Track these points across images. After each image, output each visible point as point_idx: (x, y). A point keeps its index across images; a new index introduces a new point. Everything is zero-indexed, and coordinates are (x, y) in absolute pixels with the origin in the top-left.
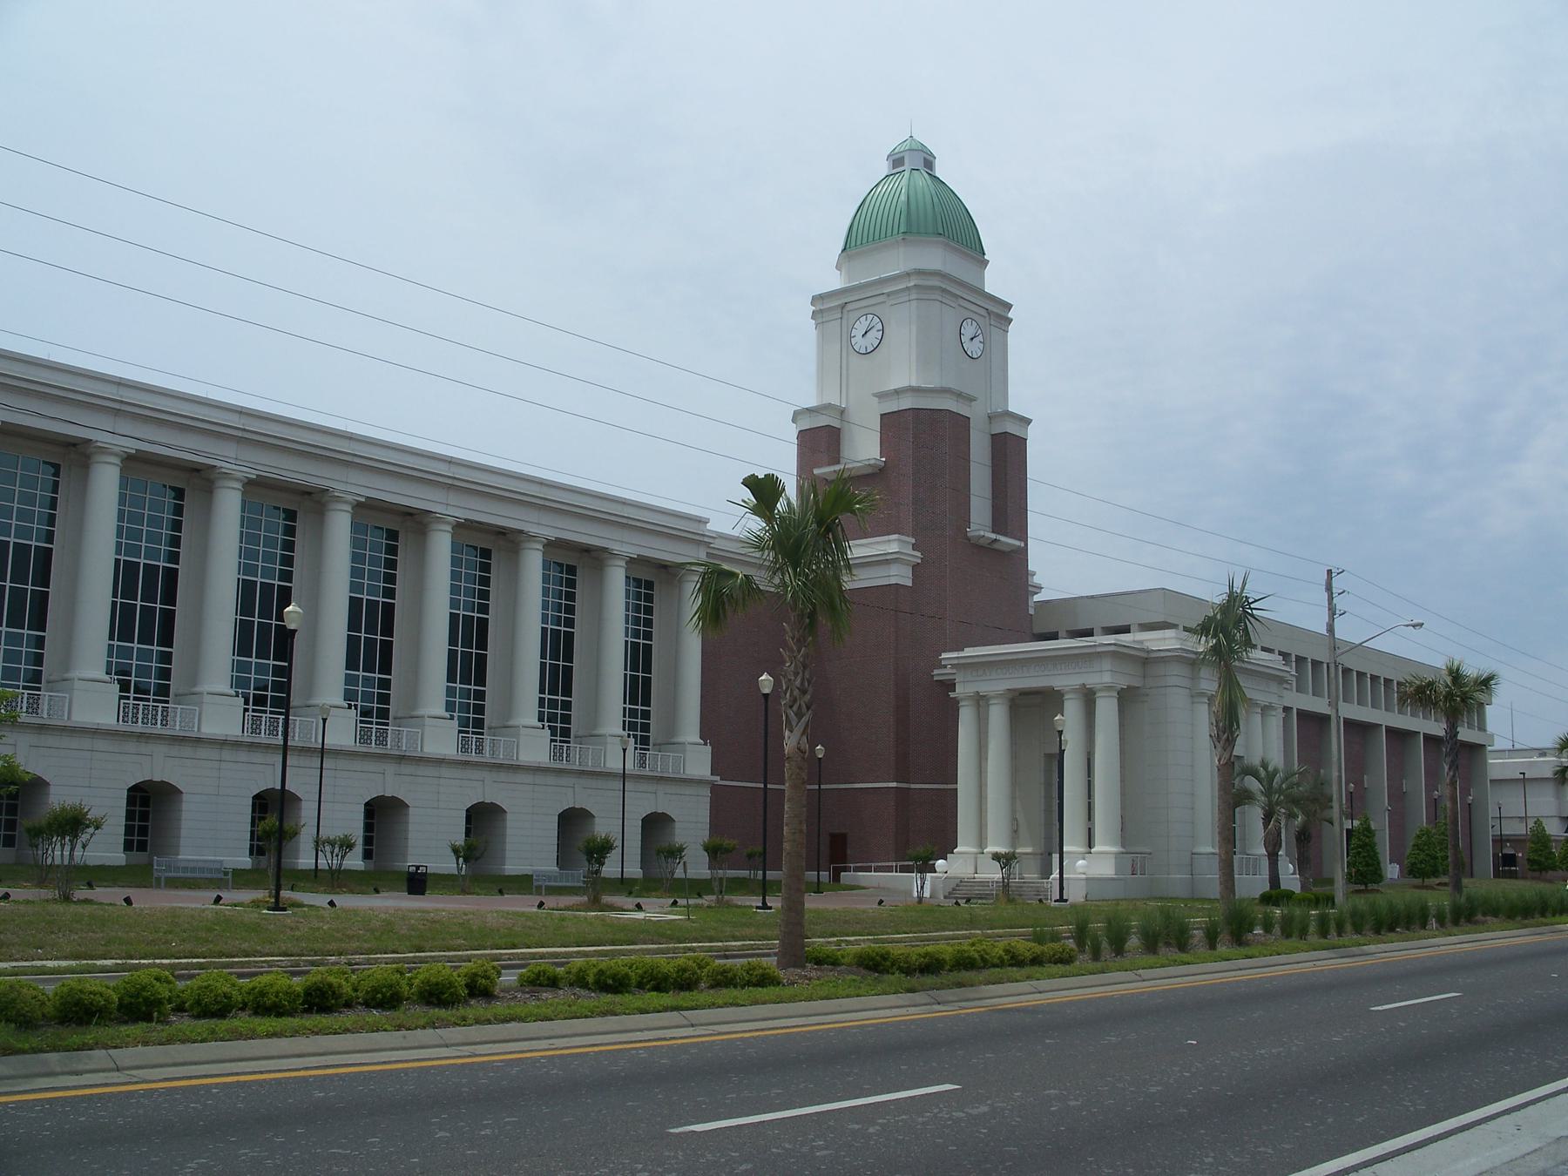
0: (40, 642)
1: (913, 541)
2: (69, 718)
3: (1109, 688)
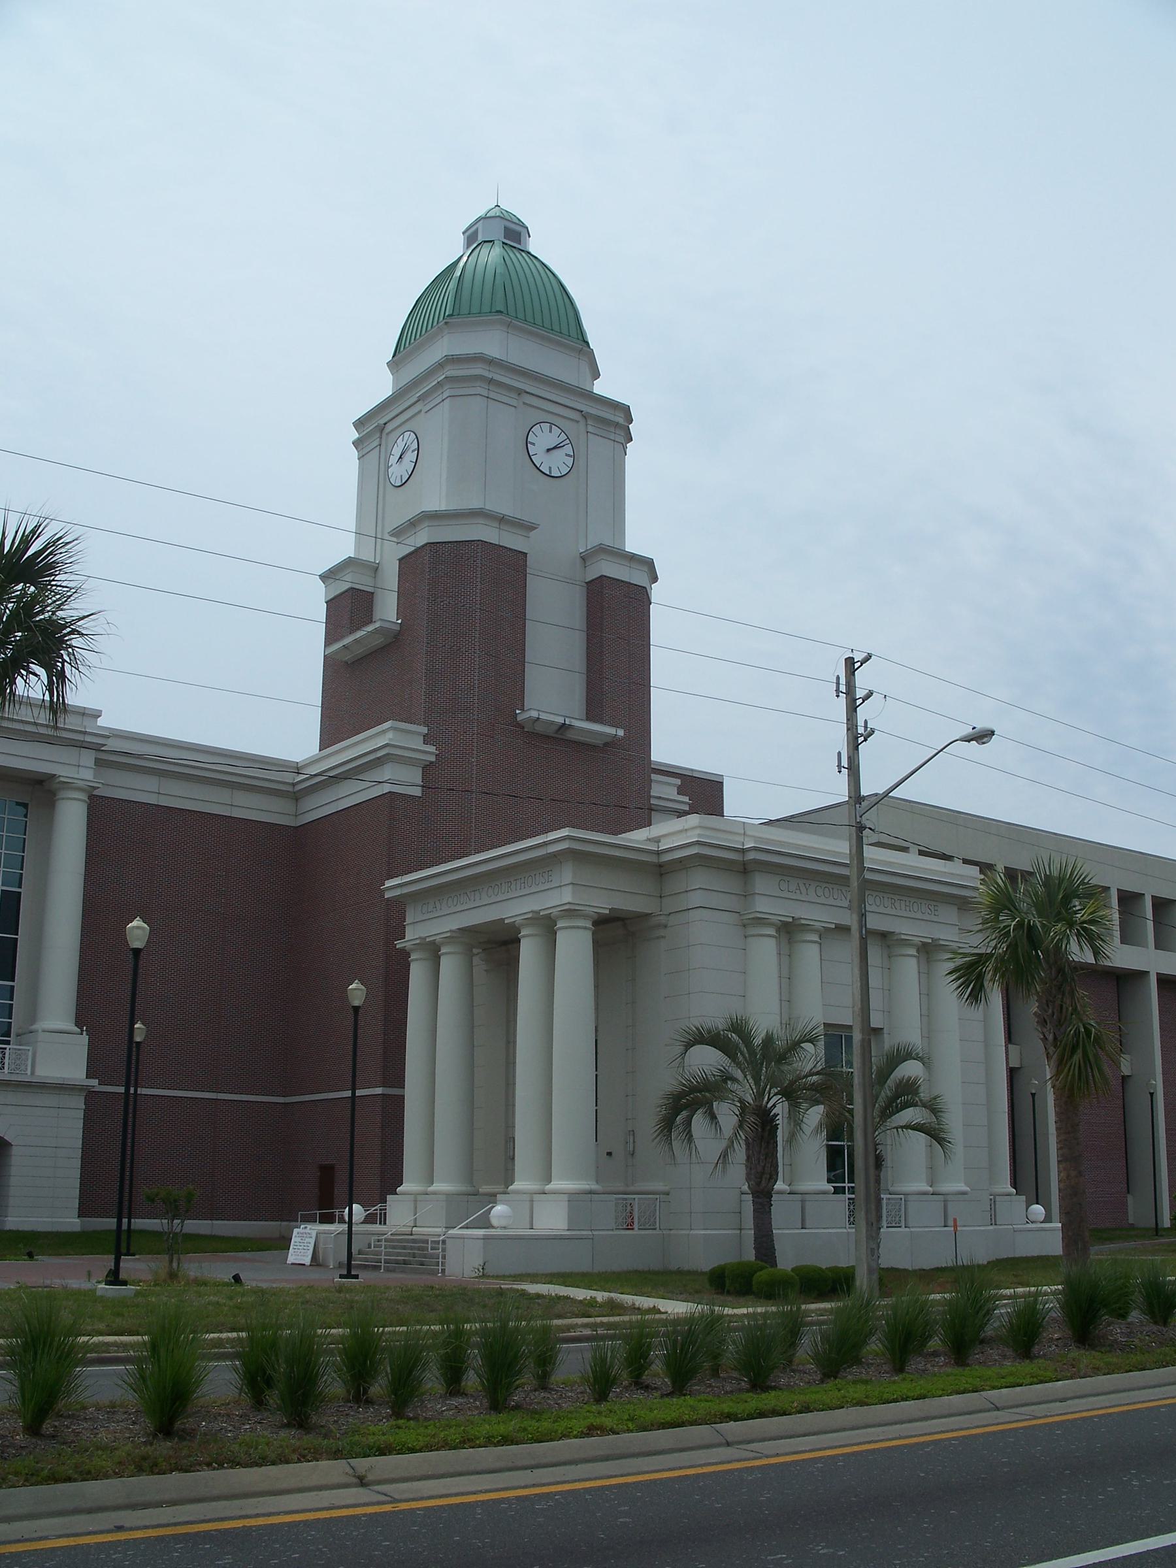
1: (425, 730)
2: (33, 1073)
3: (571, 913)
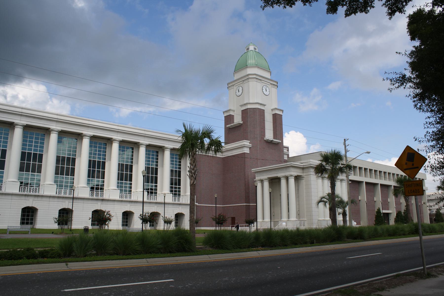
0: (131, 184)
